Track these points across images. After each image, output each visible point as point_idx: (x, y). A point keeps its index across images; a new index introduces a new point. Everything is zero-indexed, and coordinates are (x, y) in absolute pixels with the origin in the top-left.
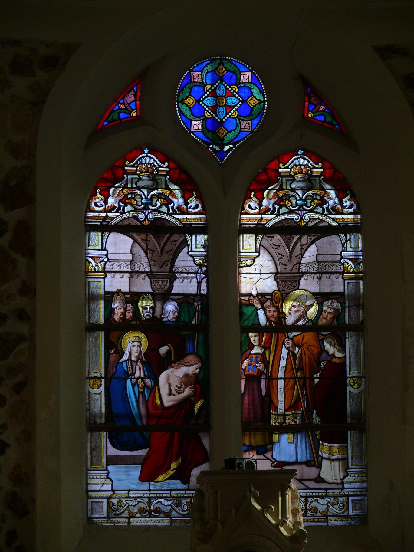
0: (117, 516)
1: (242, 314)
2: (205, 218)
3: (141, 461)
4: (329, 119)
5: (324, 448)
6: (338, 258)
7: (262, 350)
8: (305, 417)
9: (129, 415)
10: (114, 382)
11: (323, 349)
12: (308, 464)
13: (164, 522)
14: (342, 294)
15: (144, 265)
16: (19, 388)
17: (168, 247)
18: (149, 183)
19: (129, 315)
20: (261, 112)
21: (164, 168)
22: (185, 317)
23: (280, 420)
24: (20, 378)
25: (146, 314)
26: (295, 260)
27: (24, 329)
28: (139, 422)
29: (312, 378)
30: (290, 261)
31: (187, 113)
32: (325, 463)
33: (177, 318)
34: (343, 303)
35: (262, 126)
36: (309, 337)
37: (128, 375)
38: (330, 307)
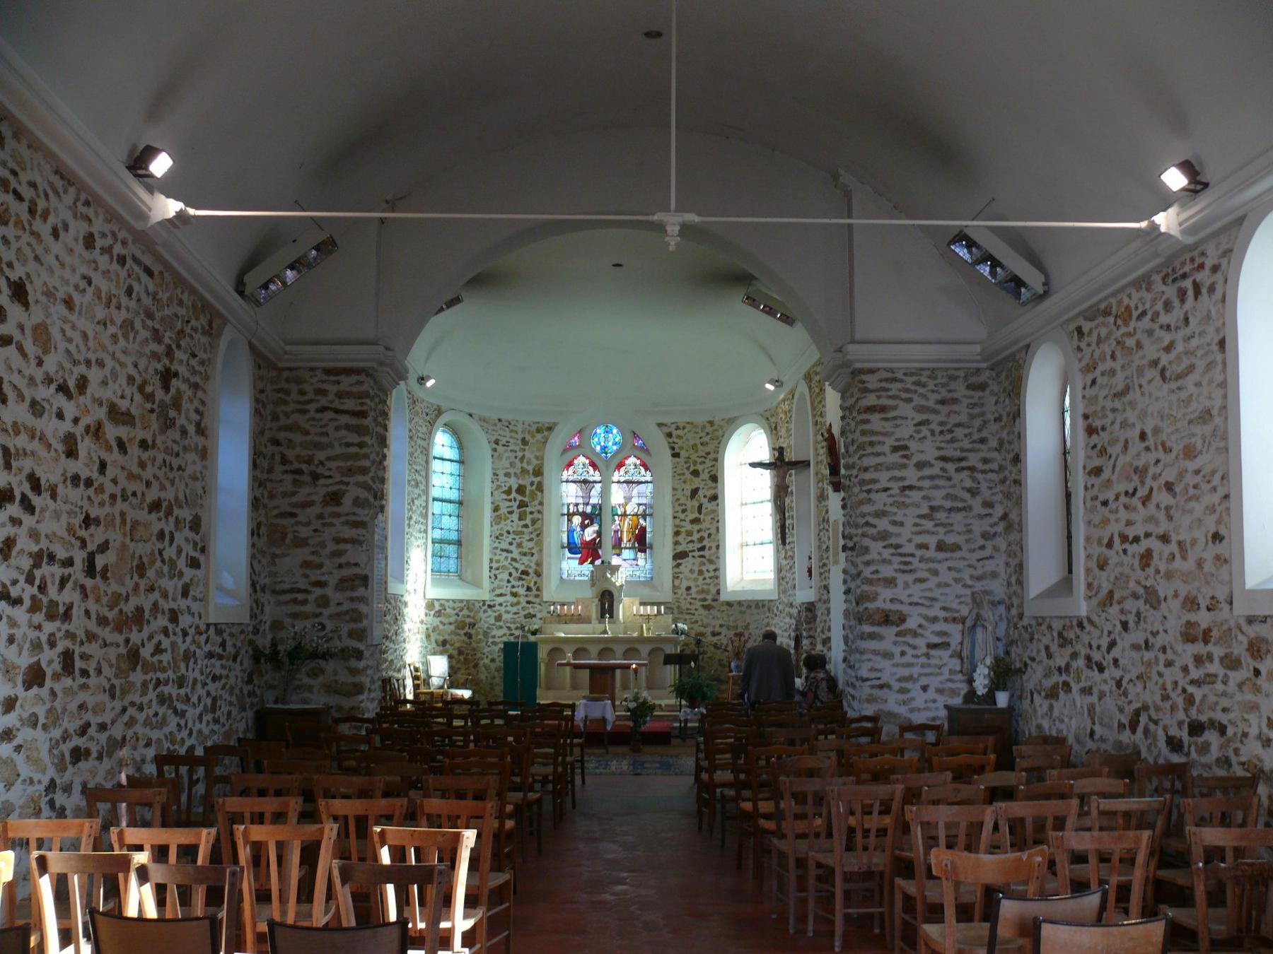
2: (677, 667)
7: (1076, 757)
15: (580, 493)
16: (538, 535)
21: (587, 461)
25: (581, 510)
27: (540, 516)
38: (642, 508)
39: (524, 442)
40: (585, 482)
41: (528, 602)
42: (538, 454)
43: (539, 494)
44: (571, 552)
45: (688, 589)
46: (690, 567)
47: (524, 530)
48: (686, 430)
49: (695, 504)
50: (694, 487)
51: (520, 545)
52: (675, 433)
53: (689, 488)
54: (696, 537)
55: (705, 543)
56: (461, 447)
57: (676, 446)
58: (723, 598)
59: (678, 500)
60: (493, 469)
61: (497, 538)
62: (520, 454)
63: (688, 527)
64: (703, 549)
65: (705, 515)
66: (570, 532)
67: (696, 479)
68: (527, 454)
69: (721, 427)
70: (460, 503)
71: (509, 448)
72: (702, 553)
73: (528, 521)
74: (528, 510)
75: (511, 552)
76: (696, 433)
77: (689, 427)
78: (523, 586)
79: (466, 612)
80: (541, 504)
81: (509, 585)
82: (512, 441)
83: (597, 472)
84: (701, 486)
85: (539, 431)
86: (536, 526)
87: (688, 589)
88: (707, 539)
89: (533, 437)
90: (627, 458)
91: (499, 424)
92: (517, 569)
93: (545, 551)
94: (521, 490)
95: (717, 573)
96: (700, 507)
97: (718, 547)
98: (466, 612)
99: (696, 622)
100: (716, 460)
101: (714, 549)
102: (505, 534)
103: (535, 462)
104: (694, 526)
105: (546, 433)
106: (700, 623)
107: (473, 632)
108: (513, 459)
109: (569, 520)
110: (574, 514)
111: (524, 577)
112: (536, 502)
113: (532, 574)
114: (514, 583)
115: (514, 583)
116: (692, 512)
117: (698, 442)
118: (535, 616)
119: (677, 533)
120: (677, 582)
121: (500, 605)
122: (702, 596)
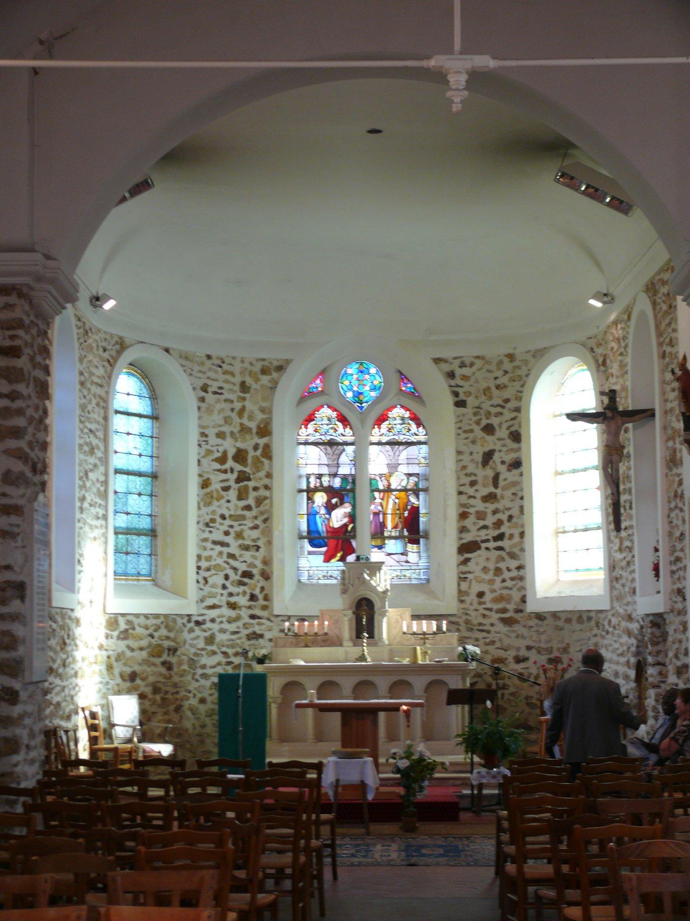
0: (312, 579)
1: (371, 484)
3: (323, 553)
4: (413, 390)
5: (410, 547)
6: (416, 457)
8: (401, 531)
9: (318, 532)
11: (409, 501)
12: (402, 554)
15: (325, 460)
16: (265, 521)
18: (327, 422)
19: (318, 485)
20: (380, 388)
21: (334, 414)
22: (344, 486)
23: (389, 533)
24: (265, 516)
26: (396, 458)
28: (322, 535)
30: (394, 458)
31: (345, 388)
32: (410, 554)
33: (341, 486)
34: (418, 478)
35: (380, 394)
36: (403, 494)
37: (317, 513)
38: (413, 479)
39: (244, 387)
40: (331, 443)
41: (253, 617)
42: (264, 404)
43: (266, 461)
44: (313, 544)
45: (481, 595)
46: (483, 563)
47: (246, 513)
48: (474, 368)
49: (490, 473)
50: (487, 449)
51: (239, 535)
52: (459, 372)
53: (479, 450)
54: (490, 520)
55: (504, 529)
56: (154, 397)
58: (530, 607)
59: (464, 467)
60: (200, 426)
61: (207, 525)
62: (238, 406)
63: (480, 506)
64: (500, 537)
65: (505, 488)
66: (311, 515)
67: (490, 438)
68: (247, 404)
70: (154, 476)
72: (499, 544)
73: (251, 501)
74: (251, 484)
75: (227, 545)
76: (489, 371)
78: (244, 593)
79: (163, 632)
80: (269, 475)
81: (225, 592)
82: (226, 386)
84: (497, 448)
85: (264, 371)
86: (262, 508)
88: (507, 524)
90: (390, 409)
91: (208, 363)
92: (235, 569)
94: (240, 456)
95: (521, 572)
97: (522, 534)
98: (163, 632)
99: (492, 643)
100: (518, 410)
101: (517, 539)
102: (219, 520)
103: (260, 416)
104: (487, 505)
105: (275, 375)
106: (498, 645)
107: (173, 660)
108: (229, 413)
110: (316, 490)
111: (246, 580)
112: (262, 474)
113: (257, 577)
114: (232, 589)
115: (232, 589)
116: (484, 486)
118: (261, 636)
119: (463, 516)
120: (464, 586)
121: (213, 621)
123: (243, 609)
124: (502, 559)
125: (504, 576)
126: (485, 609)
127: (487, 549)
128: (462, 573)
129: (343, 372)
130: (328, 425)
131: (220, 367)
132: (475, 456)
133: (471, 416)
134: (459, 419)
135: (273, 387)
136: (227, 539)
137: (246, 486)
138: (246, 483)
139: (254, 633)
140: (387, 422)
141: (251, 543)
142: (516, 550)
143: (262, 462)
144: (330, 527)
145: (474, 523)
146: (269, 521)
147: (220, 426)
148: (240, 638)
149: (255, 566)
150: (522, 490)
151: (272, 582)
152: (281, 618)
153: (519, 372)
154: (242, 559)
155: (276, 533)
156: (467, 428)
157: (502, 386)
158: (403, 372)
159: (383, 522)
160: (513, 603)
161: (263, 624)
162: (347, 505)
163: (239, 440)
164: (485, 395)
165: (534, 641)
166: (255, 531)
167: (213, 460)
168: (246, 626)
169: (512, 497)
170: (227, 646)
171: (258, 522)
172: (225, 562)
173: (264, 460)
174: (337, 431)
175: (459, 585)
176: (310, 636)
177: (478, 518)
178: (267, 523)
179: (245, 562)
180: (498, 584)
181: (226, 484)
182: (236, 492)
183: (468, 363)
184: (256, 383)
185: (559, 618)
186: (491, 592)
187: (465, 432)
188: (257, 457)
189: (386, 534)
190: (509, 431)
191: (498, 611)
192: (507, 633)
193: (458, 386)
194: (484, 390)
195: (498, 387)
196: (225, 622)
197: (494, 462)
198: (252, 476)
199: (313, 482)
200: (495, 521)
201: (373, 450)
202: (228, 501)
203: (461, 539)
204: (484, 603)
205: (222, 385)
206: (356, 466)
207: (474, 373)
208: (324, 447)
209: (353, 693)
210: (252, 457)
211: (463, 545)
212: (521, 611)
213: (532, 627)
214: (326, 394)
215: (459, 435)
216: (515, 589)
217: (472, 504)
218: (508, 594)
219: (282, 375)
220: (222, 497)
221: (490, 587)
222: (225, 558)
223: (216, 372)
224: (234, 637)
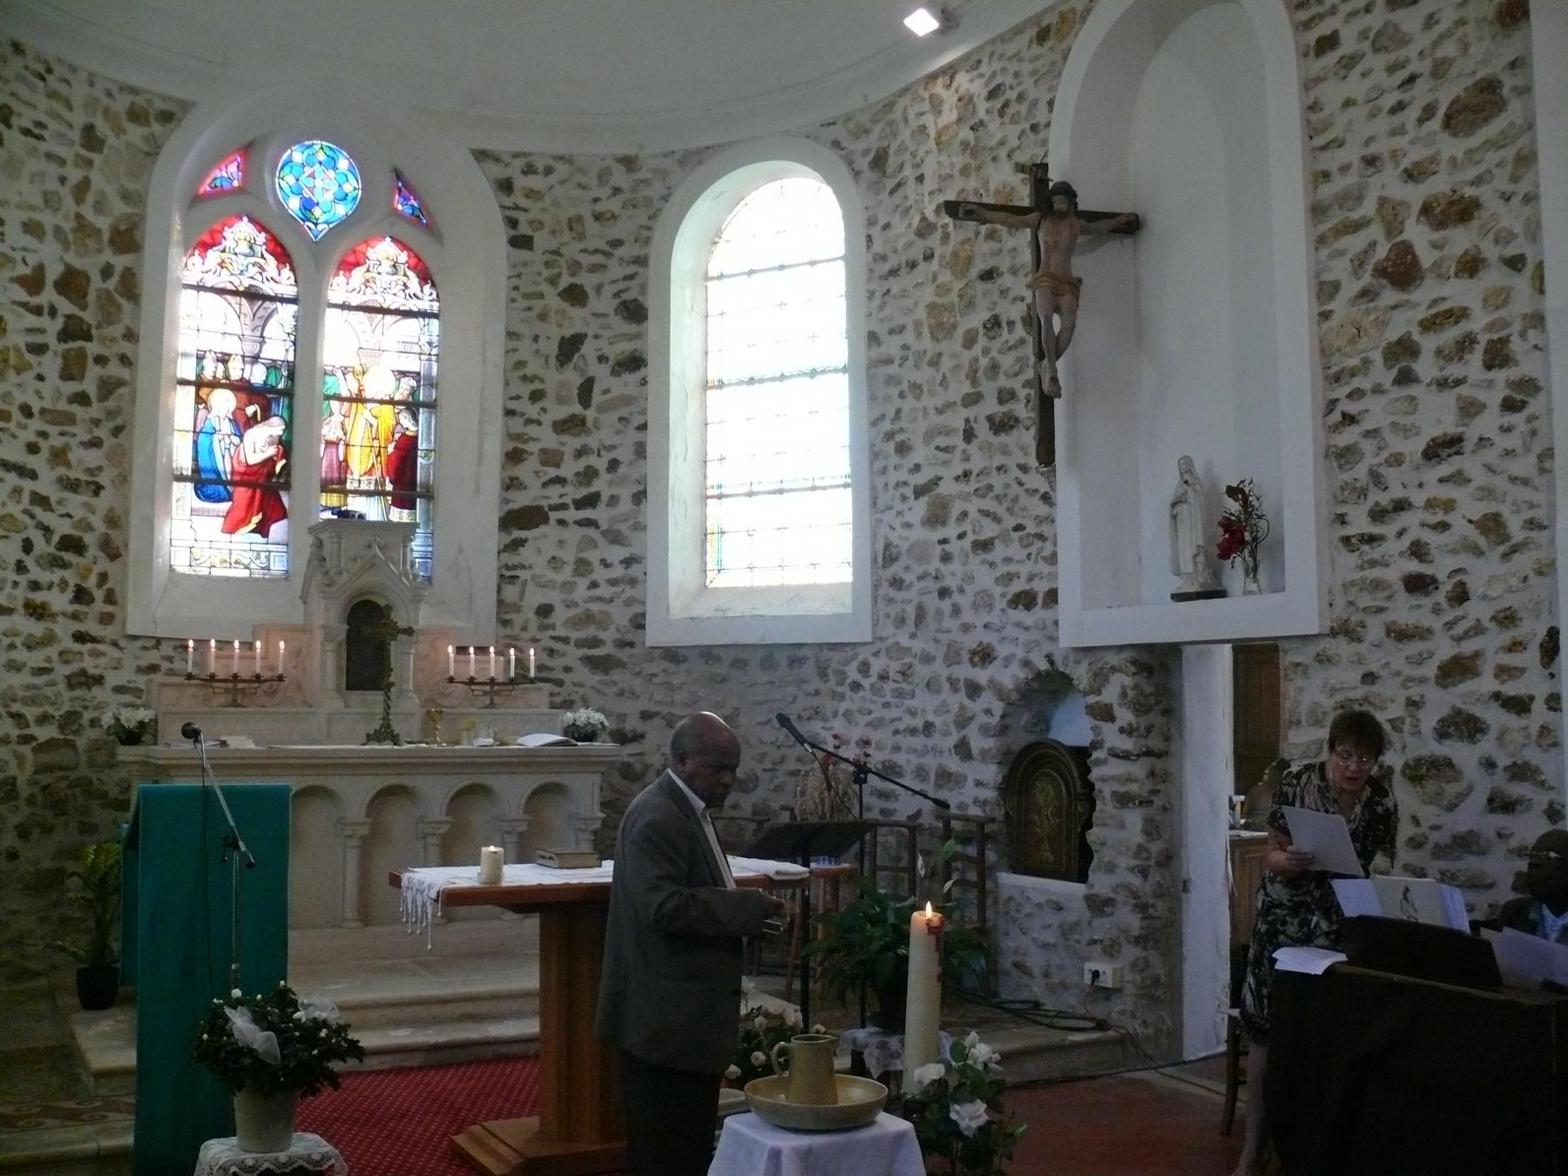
0: (198, 565)
10: (202, 437)
13: (245, 573)
14: (419, 374)
15: (234, 325)
16: (117, 431)
17: (261, 313)
19: (220, 374)
20: (355, 198)
22: (272, 381)
24: (119, 421)
27: (124, 373)
28: (223, 477)
29: (386, 448)
38: (408, 383)
39: (91, 139)
40: (252, 295)
41: (80, 637)
42: (130, 185)
44: (201, 492)
45: (545, 611)
46: (550, 550)
47: (76, 409)
48: (552, 179)
49: (573, 378)
50: (568, 333)
51: (59, 457)
52: (521, 182)
53: (552, 336)
54: (569, 468)
55: (599, 485)
57: (522, 217)
58: (655, 636)
59: (521, 364)
62: (74, 175)
63: (548, 439)
64: (591, 501)
65: (602, 409)
67: (576, 312)
69: (663, 174)
71: (43, 147)
72: (588, 513)
73: (89, 385)
74: (92, 348)
75: (33, 475)
77: (562, 169)
78: (63, 584)
80: (131, 336)
81: (23, 580)
82: (53, 125)
83: (286, 272)
84: (591, 331)
85: (136, 115)
86: (111, 403)
87: (545, 611)
88: (605, 476)
89: (119, 131)
92: (47, 530)
93: (137, 480)
94: (72, 283)
95: (635, 571)
96: (585, 391)
97: (640, 497)
100: (641, 261)
101: (626, 505)
102: (17, 416)
103: (119, 207)
104: (565, 438)
105: (157, 128)
108: (53, 185)
109: (199, 400)
110: (214, 384)
111: (68, 556)
112: (117, 330)
114: (36, 573)
115: (36, 573)
116: (561, 400)
117: (586, 211)
118: (99, 680)
119: (514, 457)
120: (511, 592)
122: (589, 632)
123: (60, 619)
124: (593, 544)
125: (594, 577)
126: (553, 638)
127: (562, 522)
128: (508, 567)
129: (285, 157)
130: (246, 256)
131: (43, 79)
132: (541, 344)
133: (540, 267)
134: (516, 271)
135: (153, 150)
136: (32, 462)
137: (82, 351)
138: (80, 343)
139: (83, 672)
140: (362, 269)
141: (84, 477)
142: (623, 528)
143: (119, 307)
144: (239, 463)
145: (536, 473)
146: (126, 430)
147: (32, 208)
148: (52, 684)
149: (89, 528)
150: (643, 412)
151: (125, 565)
152: (140, 643)
153: (647, 192)
154: (63, 511)
155: (139, 460)
156: (531, 289)
157: (608, 215)
158: (409, 174)
159: (346, 460)
160: (612, 628)
161: (103, 654)
162: (275, 420)
163: (73, 247)
164: (571, 229)
165: (659, 702)
166: (94, 452)
167: (12, 280)
168: (64, 657)
169: (620, 426)
170: (25, 701)
171: (102, 433)
172: (25, 512)
173: (122, 301)
174: (263, 270)
175: (499, 590)
176: (480, 684)
177: (545, 463)
178: (121, 436)
179: (69, 516)
180: (581, 590)
181: (37, 339)
182: (59, 362)
183: (541, 168)
184: (118, 136)
185: (718, 659)
186: (568, 606)
187: (527, 296)
188: (107, 292)
189: (349, 486)
190: (618, 301)
191: (580, 644)
192: (599, 687)
193: (517, 208)
194: (570, 221)
195: (598, 217)
196: (20, 647)
197: (583, 356)
198: (94, 332)
199: (211, 370)
200: (581, 469)
201: (332, 318)
202: (41, 378)
203: (506, 501)
204: (553, 627)
205: (44, 119)
206: (298, 344)
207: (551, 187)
208: (238, 299)
209: (368, 815)
210: (97, 290)
211: (510, 513)
212: (631, 645)
213: (655, 675)
214: (248, 193)
215: (513, 300)
216: (619, 602)
217: (533, 435)
218: (602, 612)
219: (172, 131)
220: (29, 367)
221: (564, 596)
222: (26, 501)
223: (33, 89)
224: (39, 680)
